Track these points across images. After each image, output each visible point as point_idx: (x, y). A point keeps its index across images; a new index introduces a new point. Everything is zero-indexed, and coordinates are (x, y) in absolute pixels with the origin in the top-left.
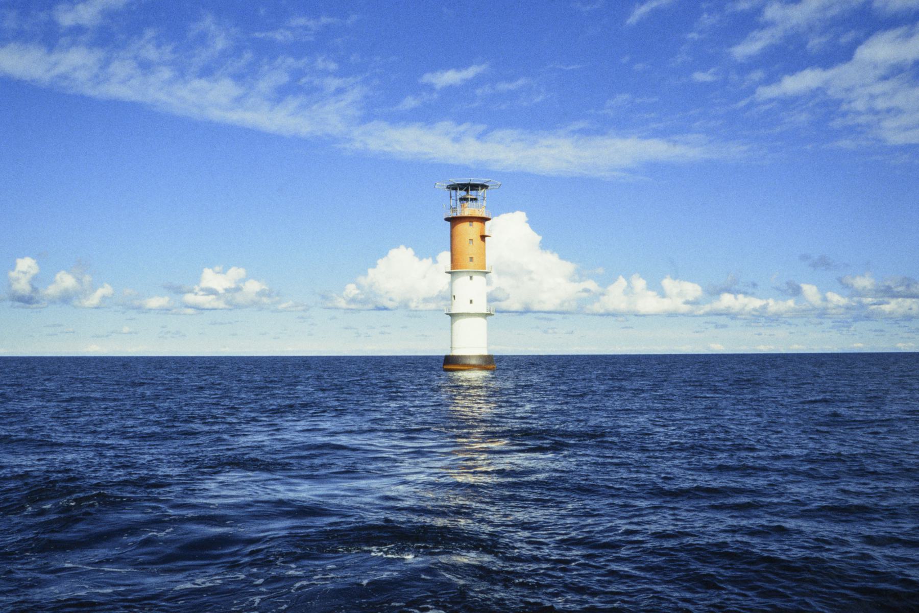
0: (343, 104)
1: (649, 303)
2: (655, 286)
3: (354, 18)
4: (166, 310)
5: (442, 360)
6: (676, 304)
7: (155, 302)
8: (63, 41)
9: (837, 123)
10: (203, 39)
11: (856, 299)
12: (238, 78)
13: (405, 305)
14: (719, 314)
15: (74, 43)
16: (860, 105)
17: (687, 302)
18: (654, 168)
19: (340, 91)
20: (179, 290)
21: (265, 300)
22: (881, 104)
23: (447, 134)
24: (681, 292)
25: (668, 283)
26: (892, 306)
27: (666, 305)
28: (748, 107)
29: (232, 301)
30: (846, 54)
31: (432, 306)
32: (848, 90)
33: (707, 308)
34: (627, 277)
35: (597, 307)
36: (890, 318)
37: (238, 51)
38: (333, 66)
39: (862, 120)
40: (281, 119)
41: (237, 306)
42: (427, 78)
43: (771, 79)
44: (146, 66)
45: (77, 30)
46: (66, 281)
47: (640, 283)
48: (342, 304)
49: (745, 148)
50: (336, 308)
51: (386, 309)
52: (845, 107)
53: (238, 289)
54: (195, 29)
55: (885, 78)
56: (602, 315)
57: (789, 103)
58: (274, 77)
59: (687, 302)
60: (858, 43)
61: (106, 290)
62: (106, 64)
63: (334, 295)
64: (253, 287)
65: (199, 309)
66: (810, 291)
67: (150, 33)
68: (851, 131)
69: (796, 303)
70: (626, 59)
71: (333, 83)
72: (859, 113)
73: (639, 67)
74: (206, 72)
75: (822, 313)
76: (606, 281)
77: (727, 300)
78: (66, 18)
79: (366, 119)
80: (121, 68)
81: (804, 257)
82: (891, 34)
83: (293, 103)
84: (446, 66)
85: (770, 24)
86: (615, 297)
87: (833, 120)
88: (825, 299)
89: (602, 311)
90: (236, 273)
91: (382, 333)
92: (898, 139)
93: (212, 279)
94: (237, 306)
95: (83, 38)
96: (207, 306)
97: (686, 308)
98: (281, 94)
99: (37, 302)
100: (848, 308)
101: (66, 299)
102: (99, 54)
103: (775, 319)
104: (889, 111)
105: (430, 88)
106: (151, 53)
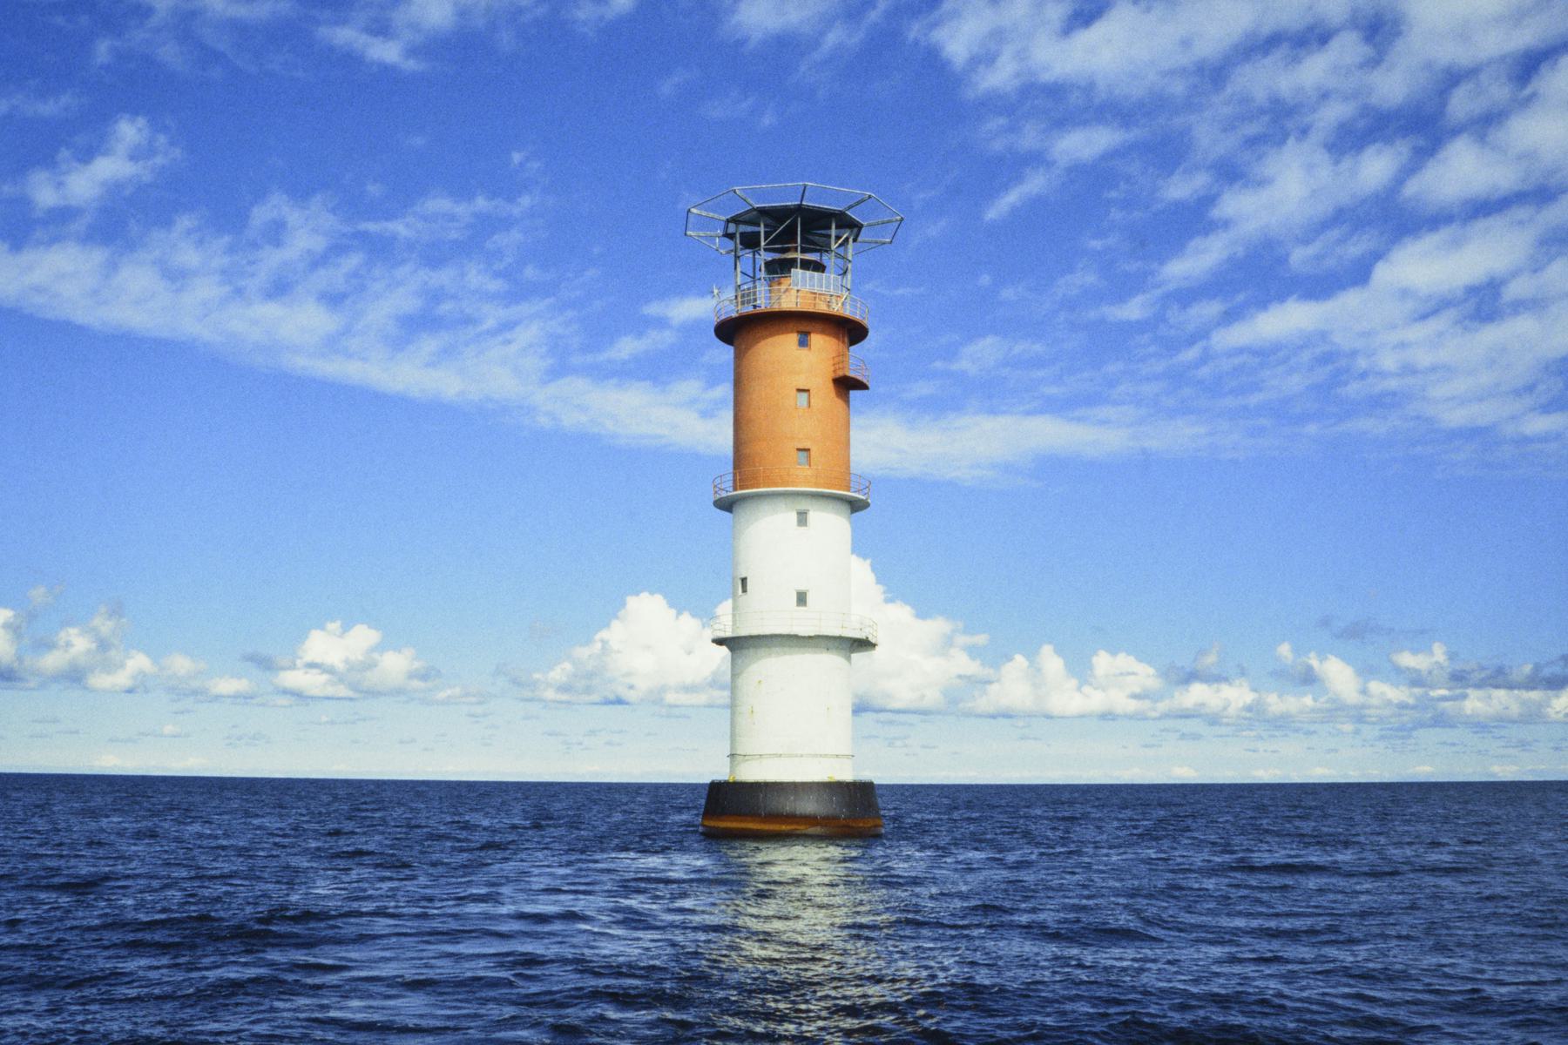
0: (513, 348)
1: (1069, 699)
2: (1080, 669)
3: (525, 201)
4: (237, 697)
5: (704, 793)
6: (1121, 701)
7: (227, 686)
8: (39, 233)
9: (1353, 389)
10: (276, 233)
11: (1417, 690)
12: (333, 300)
13: (655, 698)
14: (1186, 715)
15: (55, 240)
16: (1389, 362)
17: (1135, 696)
18: (1052, 467)
19: (508, 326)
20: (265, 664)
21: (416, 684)
22: (1424, 359)
23: (692, 402)
24: (1121, 677)
25: (1103, 662)
26: (1476, 703)
27: (1095, 700)
28: (1205, 358)
29: (358, 687)
30: (1359, 274)
31: (702, 698)
32: (1366, 334)
33: (1163, 706)
34: (1032, 655)
35: (983, 703)
36: (1480, 726)
37: (337, 249)
38: (495, 285)
39: (1392, 384)
40: (413, 374)
41: (373, 693)
42: (653, 309)
43: (1231, 317)
44: (176, 277)
45: (63, 215)
46: (78, 643)
47: (1052, 662)
48: (550, 694)
49: (1202, 430)
50: (540, 700)
51: (619, 701)
52: (1362, 363)
53: (369, 665)
54: (261, 215)
55: (1424, 317)
56: (993, 717)
57: (1266, 354)
58: (395, 297)
59: (1135, 696)
60: (1378, 256)
61: (138, 662)
62: (112, 267)
63: (537, 676)
64: (396, 664)
65: (298, 695)
66: (1339, 675)
67: (185, 222)
68: (1379, 403)
69: (1315, 700)
70: (985, 280)
71: (493, 315)
72: (1383, 375)
73: (1008, 293)
74: (279, 289)
75: (1359, 715)
76: (995, 656)
77: (1197, 693)
78: (44, 193)
79: (556, 372)
80: (138, 277)
81: (1325, 622)
82: (1430, 241)
83: (429, 344)
84: (681, 289)
85: (1226, 224)
86: (1013, 685)
87: (1346, 384)
88: (1364, 692)
89: (992, 710)
90: (363, 638)
91: (609, 743)
92: (1456, 417)
93: (331, 647)
94: (373, 693)
95: (78, 226)
96: (316, 692)
97: (1132, 706)
98: (416, 325)
99: (20, 679)
100: (1403, 706)
101: (74, 676)
102: (98, 256)
103: (1282, 724)
104: (1433, 369)
105: (661, 323)
106: (189, 256)
